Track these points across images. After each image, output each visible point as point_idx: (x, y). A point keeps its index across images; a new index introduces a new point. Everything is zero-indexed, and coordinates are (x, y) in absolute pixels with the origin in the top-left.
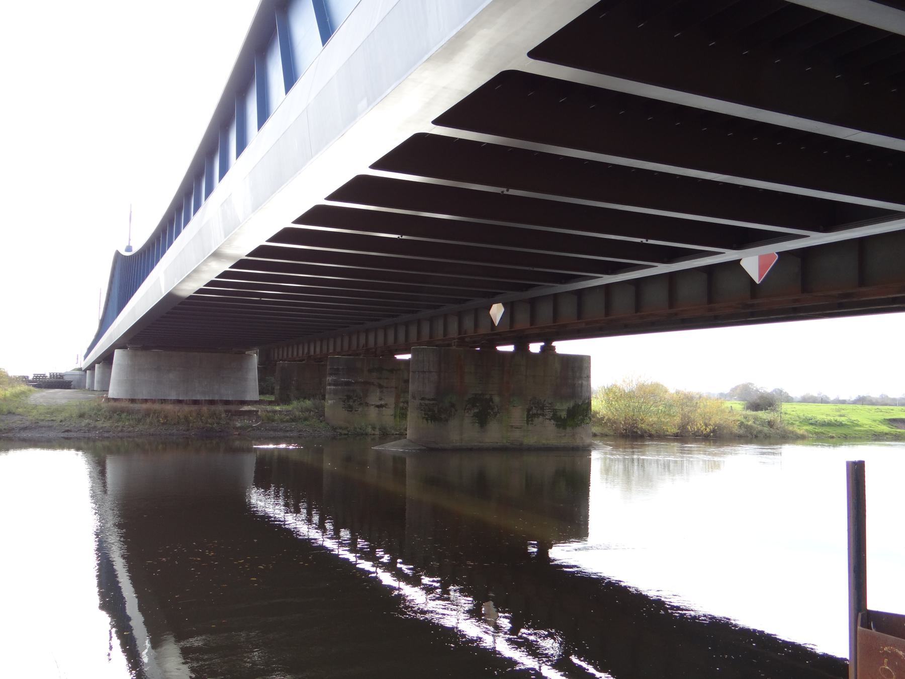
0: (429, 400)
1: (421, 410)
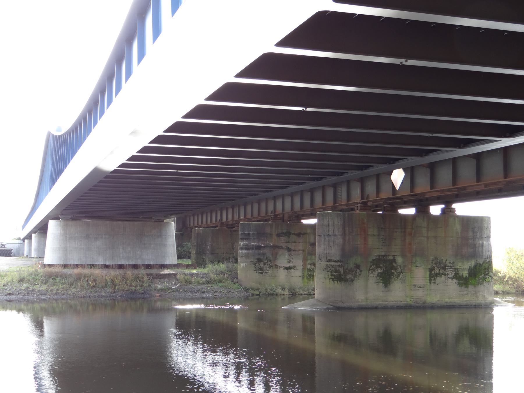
0: (335, 261)
1: (328, 271)
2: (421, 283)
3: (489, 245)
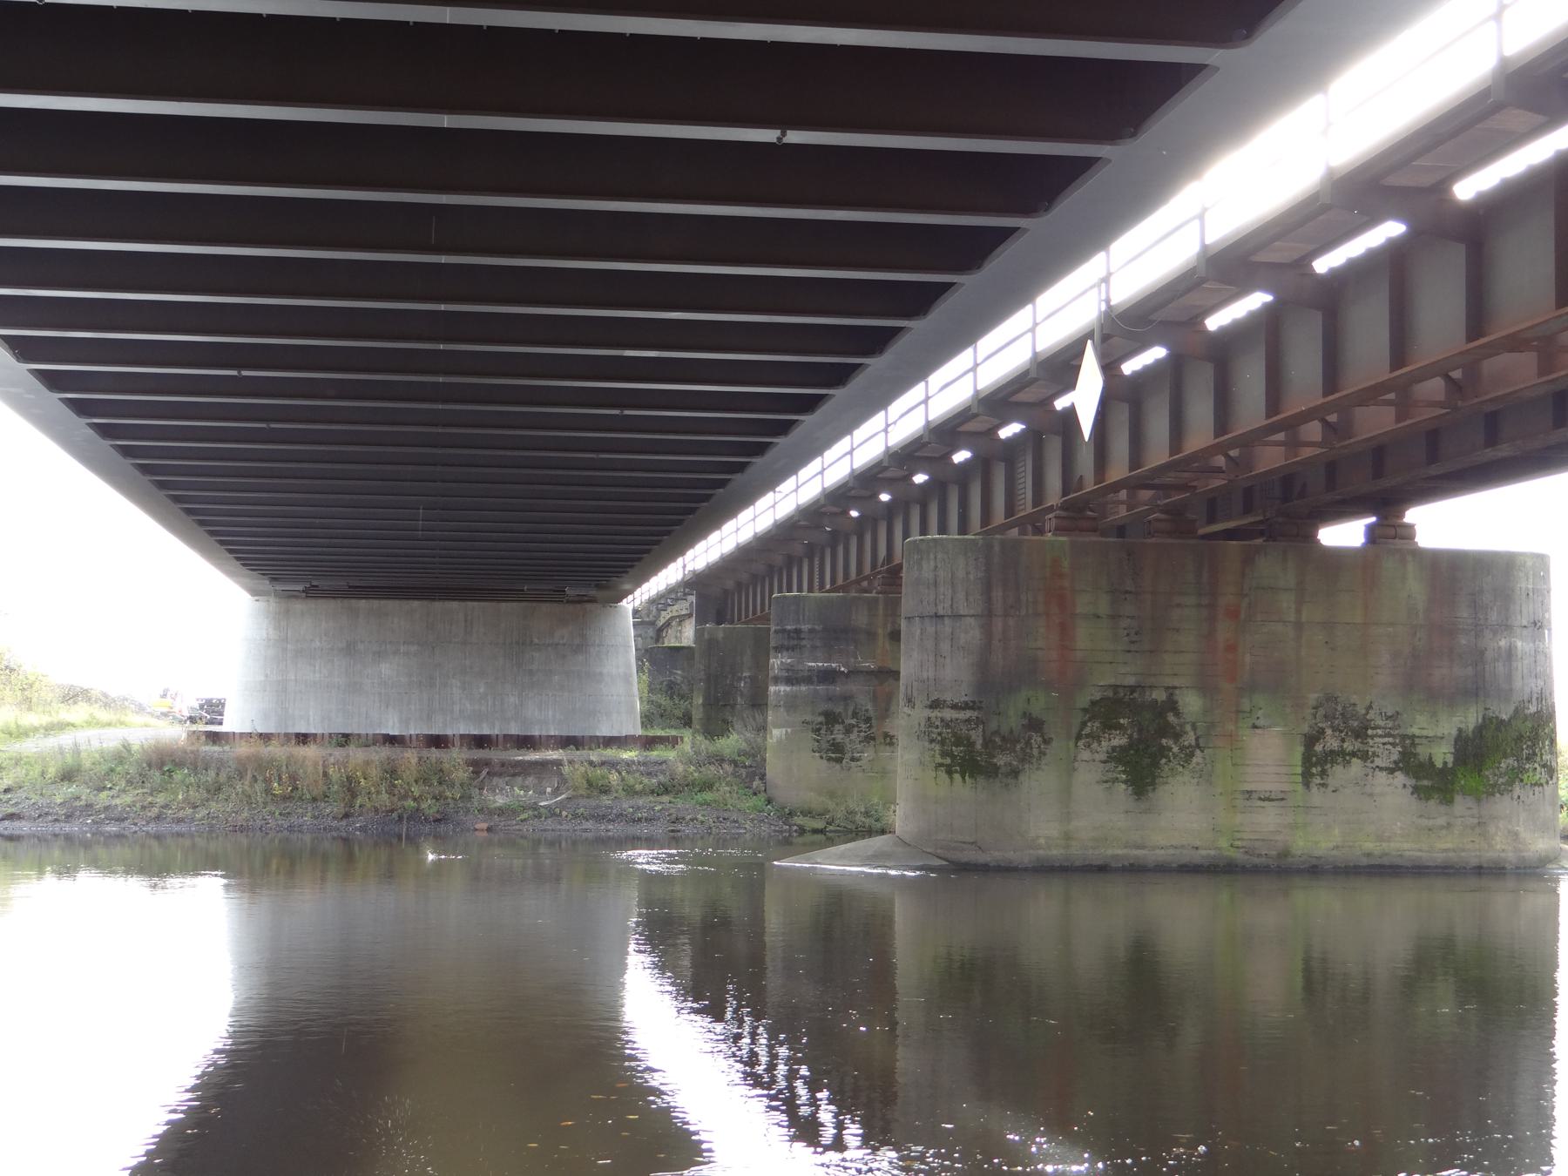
0: (955, 707)
1: (932, 741)
2: (1270, 785)
3: (1541, 658)
